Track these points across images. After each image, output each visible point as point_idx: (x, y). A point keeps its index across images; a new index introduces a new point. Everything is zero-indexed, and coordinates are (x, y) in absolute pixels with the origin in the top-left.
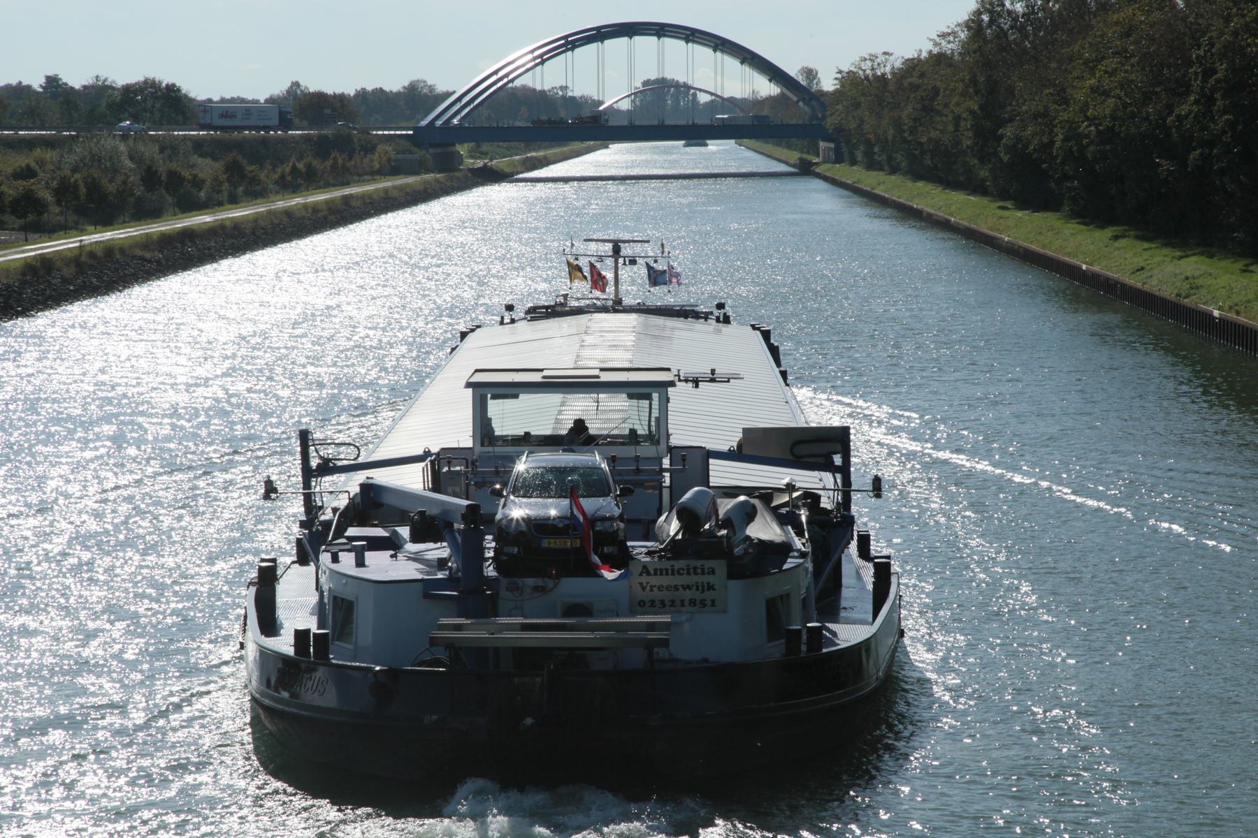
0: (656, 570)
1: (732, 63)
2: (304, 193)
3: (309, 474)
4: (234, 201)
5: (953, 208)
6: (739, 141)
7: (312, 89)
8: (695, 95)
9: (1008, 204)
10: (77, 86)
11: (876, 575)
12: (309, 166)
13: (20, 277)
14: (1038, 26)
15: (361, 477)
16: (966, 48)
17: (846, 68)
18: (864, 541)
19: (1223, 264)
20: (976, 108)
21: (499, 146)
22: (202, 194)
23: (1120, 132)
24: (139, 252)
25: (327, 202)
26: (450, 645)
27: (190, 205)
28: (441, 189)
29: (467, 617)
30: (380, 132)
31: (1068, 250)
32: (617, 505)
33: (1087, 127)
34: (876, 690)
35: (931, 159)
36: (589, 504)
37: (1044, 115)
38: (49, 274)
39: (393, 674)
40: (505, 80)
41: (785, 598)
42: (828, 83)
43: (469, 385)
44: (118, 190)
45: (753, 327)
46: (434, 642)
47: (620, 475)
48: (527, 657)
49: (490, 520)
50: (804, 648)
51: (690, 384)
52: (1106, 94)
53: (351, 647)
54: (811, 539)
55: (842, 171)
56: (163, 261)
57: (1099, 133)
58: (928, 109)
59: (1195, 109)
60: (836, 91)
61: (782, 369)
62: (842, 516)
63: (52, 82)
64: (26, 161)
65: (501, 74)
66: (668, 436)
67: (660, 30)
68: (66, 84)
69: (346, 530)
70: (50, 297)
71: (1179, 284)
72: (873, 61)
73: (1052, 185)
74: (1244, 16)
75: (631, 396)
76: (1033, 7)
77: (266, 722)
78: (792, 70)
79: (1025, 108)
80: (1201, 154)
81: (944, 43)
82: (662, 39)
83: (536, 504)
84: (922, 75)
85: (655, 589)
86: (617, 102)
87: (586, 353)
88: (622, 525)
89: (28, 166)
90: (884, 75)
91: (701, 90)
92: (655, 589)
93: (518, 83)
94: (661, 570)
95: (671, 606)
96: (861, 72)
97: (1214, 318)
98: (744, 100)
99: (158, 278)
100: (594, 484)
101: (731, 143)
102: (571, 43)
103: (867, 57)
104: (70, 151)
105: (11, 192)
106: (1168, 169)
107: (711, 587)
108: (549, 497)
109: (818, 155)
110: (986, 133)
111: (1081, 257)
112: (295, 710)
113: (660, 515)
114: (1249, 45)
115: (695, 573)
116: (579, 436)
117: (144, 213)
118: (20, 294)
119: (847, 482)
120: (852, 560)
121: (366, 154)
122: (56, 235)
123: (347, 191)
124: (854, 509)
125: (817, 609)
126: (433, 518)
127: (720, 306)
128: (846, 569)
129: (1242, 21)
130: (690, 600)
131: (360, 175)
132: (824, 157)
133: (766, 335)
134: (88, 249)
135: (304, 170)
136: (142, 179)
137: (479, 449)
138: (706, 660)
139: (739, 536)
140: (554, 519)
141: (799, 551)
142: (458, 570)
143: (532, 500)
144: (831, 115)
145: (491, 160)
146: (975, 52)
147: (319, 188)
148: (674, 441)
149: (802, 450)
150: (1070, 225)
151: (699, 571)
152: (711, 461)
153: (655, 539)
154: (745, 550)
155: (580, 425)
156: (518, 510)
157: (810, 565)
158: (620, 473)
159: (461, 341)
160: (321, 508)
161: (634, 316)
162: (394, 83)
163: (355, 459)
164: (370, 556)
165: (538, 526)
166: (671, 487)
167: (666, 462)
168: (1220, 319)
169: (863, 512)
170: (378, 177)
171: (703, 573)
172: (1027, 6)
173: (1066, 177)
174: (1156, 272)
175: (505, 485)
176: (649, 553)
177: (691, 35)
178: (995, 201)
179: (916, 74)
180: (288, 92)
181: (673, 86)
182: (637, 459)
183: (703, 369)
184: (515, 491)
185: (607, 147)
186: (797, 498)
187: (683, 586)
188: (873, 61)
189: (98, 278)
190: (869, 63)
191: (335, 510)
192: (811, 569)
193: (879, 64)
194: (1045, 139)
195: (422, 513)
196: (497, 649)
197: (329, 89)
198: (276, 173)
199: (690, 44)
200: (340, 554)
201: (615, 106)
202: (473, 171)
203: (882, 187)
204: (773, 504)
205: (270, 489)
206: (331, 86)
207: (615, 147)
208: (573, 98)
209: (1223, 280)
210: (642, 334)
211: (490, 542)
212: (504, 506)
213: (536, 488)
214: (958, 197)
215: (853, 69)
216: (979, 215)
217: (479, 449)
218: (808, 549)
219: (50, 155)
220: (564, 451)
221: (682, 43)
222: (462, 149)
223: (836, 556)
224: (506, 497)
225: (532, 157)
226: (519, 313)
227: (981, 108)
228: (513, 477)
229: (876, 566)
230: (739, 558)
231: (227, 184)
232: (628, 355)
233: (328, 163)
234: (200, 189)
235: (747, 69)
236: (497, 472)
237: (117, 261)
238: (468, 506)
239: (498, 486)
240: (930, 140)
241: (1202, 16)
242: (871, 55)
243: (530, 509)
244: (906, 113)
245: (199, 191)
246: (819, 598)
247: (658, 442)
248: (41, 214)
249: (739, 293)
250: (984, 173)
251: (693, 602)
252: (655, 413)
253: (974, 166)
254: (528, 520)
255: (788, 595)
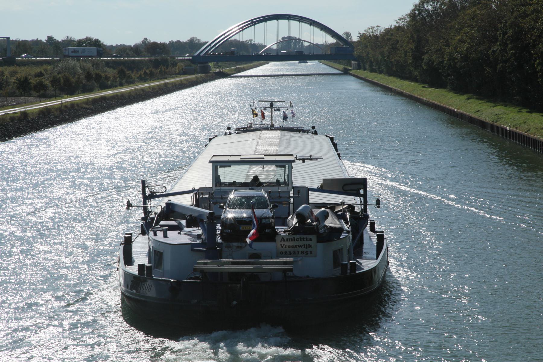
0: (287, 239)
1: (317, 30)
2: (149, 82)
3: (146, 198)
4: (121, 85)
5: (404, 87)
6: (320, 61)
7: (152, 41)
8: (302, 43)
9: (426, 86)
10: (60, 40)
11: (378, 239)
12: (151, 71)
13: (37, 115)
14: (438, 15)
15: (166, 199)
16: (409, 25)
17: (362, 32)
18: (373, 225)
19: (510, 109)
20: (413, 47)
21: (225, 63)
22: (109, 83)
23: (470, 57)
24: (84, 106)
25: (158, 86)
26: (202, 271)
27: (104, 87)
28: (203, 80)
29: (209, 259)
30: (179, 58)
31: (449, 103)
32: (271, 212)
33: (457, 55)
34: (378, 288)
35: (396, 68)
36: (259, 212)
37: (440, 50)
38: (49, 114)
39: (178, 283)
40: (228, 37)
41: (341, 250)
42: (355, 38)
43: (210, 162)
44: (76, 81)
45: (327, 136)
46: (195, 270)
47: (272, 199)
48: (235, 276)
49: (218, 218)
50: (349, 271)
51: (301, 161)
52: (464, 42)
53: (161, 271)
54: (351, 225)
55: (360, 73)
56: (94, 109)
57: (462, 58)
58: (394, 48)
59: (499, 48)
60: (358, 41)
61: (338, 153)
62: (364, 215)
63: (50, 38)
64: (40, 70)
65: (226, 35)
66: (292, 183)
67: (289, 17)
68: (55, 39)
69: (160, 222)
70: (50, 124)
71: (493, 117)
72: (373, 29)
73: (443, 78)
74: (519, 11)
75: (277, 166)
76: (436, 8)
77: (126, 302)
78: (341, 33)
79: (433, 47)
80: (502, 66)
81: (401, 22)
82: (290, 21)
83: (238, 212)
84: (392, 35)
85: (287, 247)
86: (272, 46)
87: (259, 147)
88: (273, 220)
89: (41, 72)
90: (377, 35)
91: (305, 41)
92: (287, 247)
93: (233, 38)
94: (289, 239)
95: (294, 254)
96: (368, 34)
97: (507, 130)
98: (322, 45)
99: (92, 116)
100: (261, 203)
101: (317, 61)
102: (253, 22)
103: (370, 28)
104: (57, 66)
105: (34, 82)
106: (489, 72)
107: (310, 246)
108: (243, 209)
109: (351, 67)
110: (417, 57)
111: (455, 107)
112: (138, 298)
113: (289, 216)
114: (521, 23)
115: (304, 240)
116: (256, 183)
117: (86, 90)
118: (38, 122)
119: (365, 201)
120: (367, 233)
121: (173, 67)
122: (52, 99)
123: (166, 81)
124: (369, 212)
125: (354, 253)
126: (195, 217)
127: (313, 128)
128: (365, 236)
129: (518, 13)
130: (302, 252)
131: (171, 75)
132: (353, 67)
133: (332, 139)
134: (64, 104)
135: (149, 73)
136: (85, 77)
137: (214, 188)
138: (308, 277)
139: (322, 225)
140: (245, 218)
141: (346, 230)
142: (205, 239)
143: (236, 210)
144: (356, 51)
145: (223, 69)
146: (413, 26)
147: (155, 80)
148: (295, 184)
149: (347, 188)
150: (450, 94)
151: (305, 239)
152: (310, 192)
153: (287, 225)
154: (324, 231)
155: (256, 178)
156: (230, 214)
157: (351, 236)
158: (273, 198)
159: (210, 141)
160: (151, 212)
161: (279, 132)
162: (184, 39)
163: (165, 192)
164: (169, 233)
165: (239, 221)
166: (293, 203)
167: (291, 194)
168: (509, 131)
169: (372, 215)
170: (178, 76)
171: (307, 240)
172: (433, 8)
173: (449, 75)
174: (484, 112)
175: (225, 203)
176: (285, 232)
177: (301, 19)
178: (421, 84)
179: (390, 34)
180: (143, 42)
181: (293, 39)
182: (279, 192)
183: (306, 155)
184: (229, 206)
185: (268, 64)
186: (345, 208)
187: (298, 246)
188: (373, 29)
189: (68, 116)
190: (371, 30)
191: (155, 214)
192: (351, 238)
193: (375, 31)
194: (440, 60)
195: (191, 216)
196: (222, 273)
197: (159, 41)
198: (137, 74)
199: (301, 23)
200: (157, 232)
201: (271, 47)
202: (215, 73)
203: (376, 79)
204: (336, 211)
205: (129, 205)
206: (160, 39)
207: (271, 64)
208: (254, 44)
209: (511, 115)
210: (281, 138)
211: (219, 226)
212: (225, 212)
213: (238, 205)
214: (406, 83)
215: (364, 32)
216: (414, 90)
217: (214, 188)
218: (350, 230)
219: (49, 67)
220: (249, 189)
221: (297, 22)
222: (211, 65)
223: (361, 231)
224: (225, 209)
225: (238, 68)
226: (232, 131)
227: (415, 48)
228: (228, 201)
229: (378, 235)
230: (322, 234)
231: (119, 79)
232: (276, 148)
233: (158, 70)
234: (108, 81)
235: (323, 33)
236: (222, 198)
237: (76, 109)
238: (210, 213)
239: (222, 204)
240: (395, 60)
241: (502, 11)
242: (372, 27)
243: (235, 214)
244: (385, 50)
245: (108, 81)
246: (355, 249)
247: (288, 185)
248: (45, 91)
249: (319, 121)
250: (416, 73)
251: (303, 252)
252: (287, 173)
253: (412, 71)
254: (235, 219)
255: (342, 249)
